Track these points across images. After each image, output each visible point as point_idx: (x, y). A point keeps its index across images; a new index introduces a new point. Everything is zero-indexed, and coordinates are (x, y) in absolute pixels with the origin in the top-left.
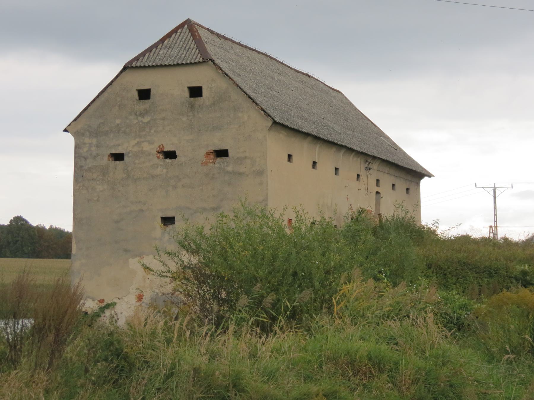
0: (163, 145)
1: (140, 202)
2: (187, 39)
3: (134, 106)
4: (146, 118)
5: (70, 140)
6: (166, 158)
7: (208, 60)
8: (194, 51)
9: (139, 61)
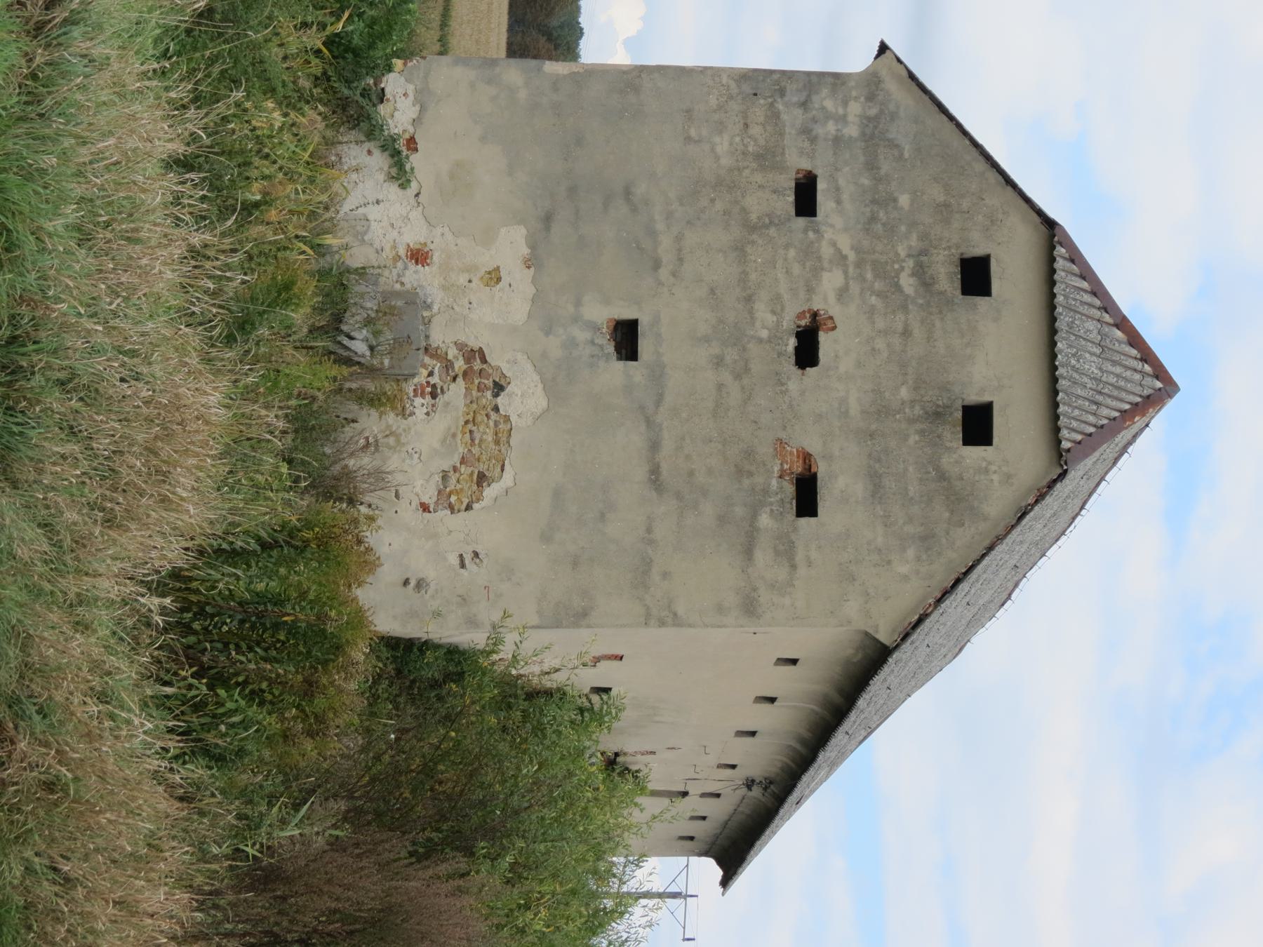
0: (834, 328)
1: (681, 260)
2: (1123, 395)
3: (945, 249)
4: (912, 281)
5: (857, 60)
6: (799, 335)
7: (1065, 467)
8: (1091, 419)
9: (1069, 265)
